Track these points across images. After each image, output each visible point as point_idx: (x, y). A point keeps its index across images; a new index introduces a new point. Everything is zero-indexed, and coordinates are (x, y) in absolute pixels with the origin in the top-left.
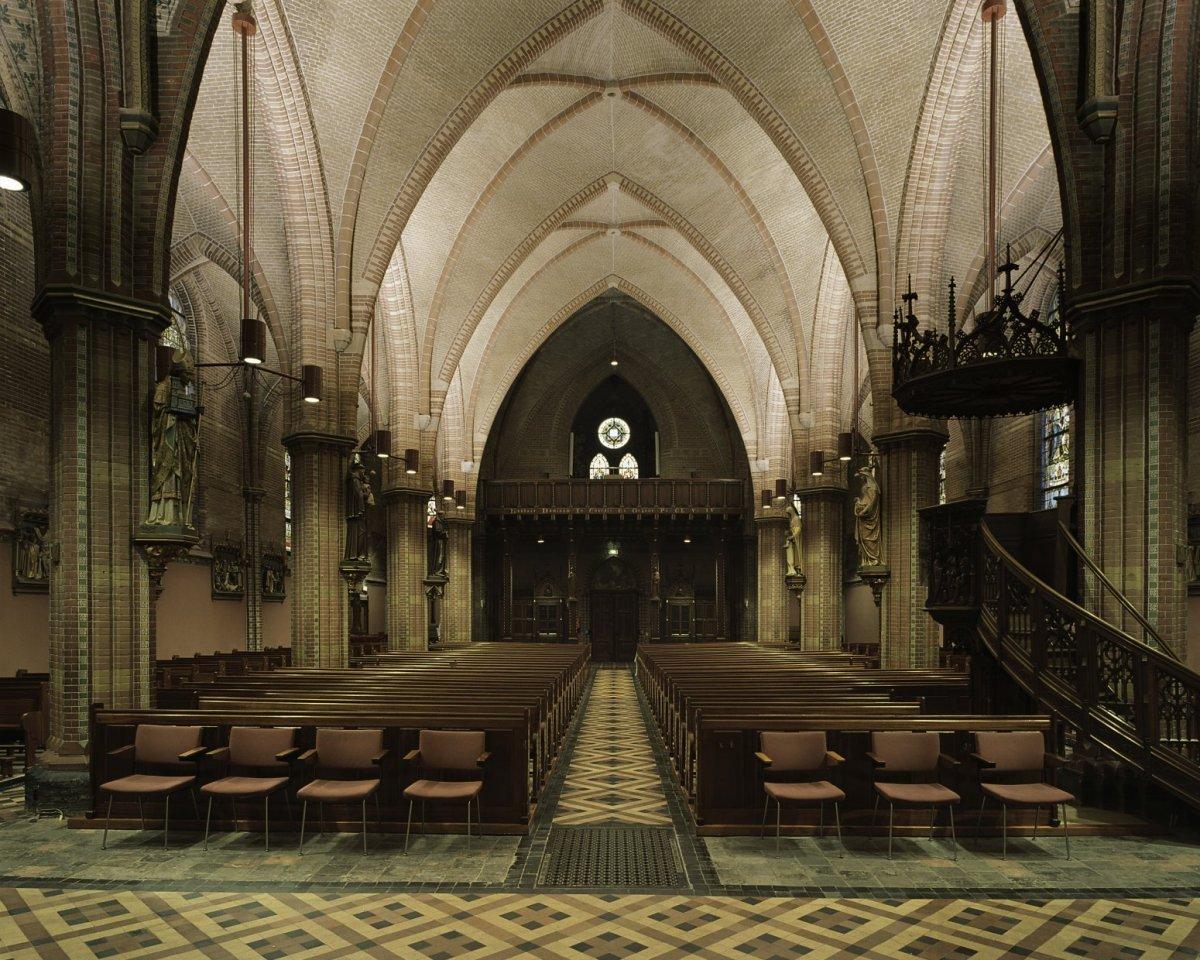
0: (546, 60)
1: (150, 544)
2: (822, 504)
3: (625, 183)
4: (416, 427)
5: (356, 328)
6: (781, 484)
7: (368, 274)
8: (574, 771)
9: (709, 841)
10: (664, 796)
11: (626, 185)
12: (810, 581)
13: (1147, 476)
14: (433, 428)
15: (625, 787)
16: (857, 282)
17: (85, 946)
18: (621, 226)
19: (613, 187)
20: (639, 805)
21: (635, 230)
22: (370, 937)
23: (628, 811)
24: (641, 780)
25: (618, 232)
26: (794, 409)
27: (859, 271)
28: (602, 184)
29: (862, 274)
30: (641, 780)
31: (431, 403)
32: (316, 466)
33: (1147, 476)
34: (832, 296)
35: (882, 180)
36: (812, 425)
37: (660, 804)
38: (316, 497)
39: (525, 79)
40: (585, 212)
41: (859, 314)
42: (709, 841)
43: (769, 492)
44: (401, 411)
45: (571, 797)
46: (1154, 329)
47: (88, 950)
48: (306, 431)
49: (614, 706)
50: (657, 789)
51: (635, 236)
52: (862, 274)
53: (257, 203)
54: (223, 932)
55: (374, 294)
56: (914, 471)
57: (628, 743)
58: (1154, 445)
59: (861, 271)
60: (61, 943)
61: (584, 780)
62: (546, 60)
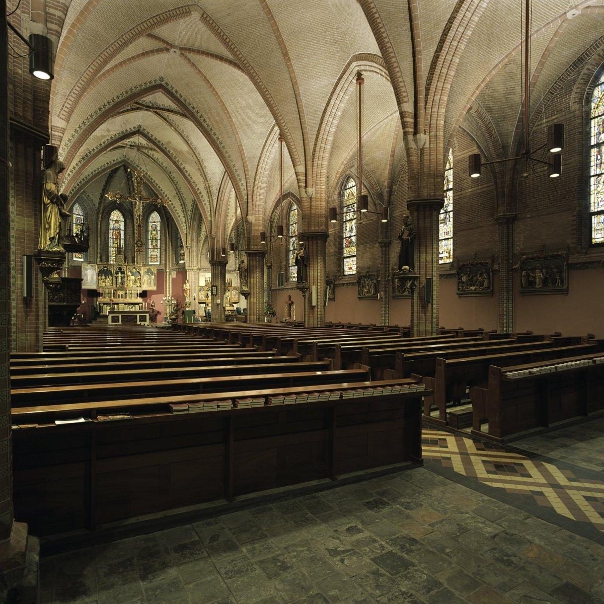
1: (52, 284)
2: (258, 258)
3: (205, 16)
11: (206, 18)
13: (432, 260)
17: (532, 476)
18: (181, 49)
19: (196, 16)
22: (551, 490)
25: (178, 51)
33: (432, 260)
35: (250, 173)
40: (164, 31)
47: (449, 445)
51: (186, 58)
54: (544, 490)
58: (319, 268)
60: (457, 451)
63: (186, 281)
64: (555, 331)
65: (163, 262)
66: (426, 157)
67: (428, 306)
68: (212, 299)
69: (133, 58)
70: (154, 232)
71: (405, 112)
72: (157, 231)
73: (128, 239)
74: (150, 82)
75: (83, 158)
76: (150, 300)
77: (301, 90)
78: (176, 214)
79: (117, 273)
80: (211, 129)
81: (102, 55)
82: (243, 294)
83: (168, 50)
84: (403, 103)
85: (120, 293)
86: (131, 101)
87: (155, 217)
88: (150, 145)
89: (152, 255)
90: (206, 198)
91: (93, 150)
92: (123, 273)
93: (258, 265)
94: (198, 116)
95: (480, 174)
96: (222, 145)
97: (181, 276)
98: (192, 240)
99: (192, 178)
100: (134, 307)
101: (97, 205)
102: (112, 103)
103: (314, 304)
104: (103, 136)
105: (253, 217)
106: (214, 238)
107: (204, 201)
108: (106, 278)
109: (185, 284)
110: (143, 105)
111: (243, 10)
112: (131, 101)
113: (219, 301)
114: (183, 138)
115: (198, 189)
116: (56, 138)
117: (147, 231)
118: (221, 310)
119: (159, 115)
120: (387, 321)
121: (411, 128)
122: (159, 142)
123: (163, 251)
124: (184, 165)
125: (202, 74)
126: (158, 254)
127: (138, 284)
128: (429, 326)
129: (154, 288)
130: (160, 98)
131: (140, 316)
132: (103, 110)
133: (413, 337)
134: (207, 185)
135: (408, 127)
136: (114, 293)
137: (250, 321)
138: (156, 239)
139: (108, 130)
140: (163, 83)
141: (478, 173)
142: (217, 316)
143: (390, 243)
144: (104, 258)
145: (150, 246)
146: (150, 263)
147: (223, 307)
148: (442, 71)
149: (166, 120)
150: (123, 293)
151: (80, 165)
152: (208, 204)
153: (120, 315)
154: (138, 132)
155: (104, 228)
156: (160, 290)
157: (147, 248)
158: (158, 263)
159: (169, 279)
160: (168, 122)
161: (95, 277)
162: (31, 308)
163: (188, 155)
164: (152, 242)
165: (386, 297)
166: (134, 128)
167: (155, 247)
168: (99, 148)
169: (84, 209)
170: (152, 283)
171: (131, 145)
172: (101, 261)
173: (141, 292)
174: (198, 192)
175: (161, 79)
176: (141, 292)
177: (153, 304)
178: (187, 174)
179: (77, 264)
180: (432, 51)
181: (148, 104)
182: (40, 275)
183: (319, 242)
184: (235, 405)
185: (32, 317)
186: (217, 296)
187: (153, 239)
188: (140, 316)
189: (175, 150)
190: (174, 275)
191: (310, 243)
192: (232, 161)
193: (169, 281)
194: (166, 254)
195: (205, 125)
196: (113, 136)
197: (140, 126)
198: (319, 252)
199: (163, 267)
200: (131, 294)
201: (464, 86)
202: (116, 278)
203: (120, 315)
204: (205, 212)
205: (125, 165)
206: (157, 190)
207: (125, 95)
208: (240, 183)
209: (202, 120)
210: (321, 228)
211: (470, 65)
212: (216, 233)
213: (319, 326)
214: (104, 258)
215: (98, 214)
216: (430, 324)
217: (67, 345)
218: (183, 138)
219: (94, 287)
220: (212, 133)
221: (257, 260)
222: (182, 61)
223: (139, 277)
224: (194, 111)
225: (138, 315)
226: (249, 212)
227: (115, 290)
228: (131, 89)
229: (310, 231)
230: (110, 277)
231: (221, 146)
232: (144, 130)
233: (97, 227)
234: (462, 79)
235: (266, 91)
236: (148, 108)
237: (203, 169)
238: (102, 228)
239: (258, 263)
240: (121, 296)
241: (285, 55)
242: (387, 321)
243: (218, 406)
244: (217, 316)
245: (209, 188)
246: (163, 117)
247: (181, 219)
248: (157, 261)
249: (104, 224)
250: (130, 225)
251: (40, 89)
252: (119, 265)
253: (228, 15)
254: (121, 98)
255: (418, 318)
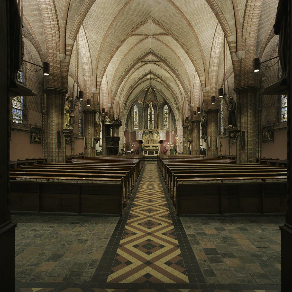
0: (137, 32)
1: (97, 139)
2: (196, 123)
4: (92, 92)
5: (67, 54)
6: (199, 109)
7: (70, 37)
8: (143, 177)
9: (181, 219)
10: (164, 193)
11: (155, 21)
12: (193, 141)
14: (97, 92)
15: (153, 197)
16: (201, 78)
18: (152, 36)
19: (150, 21)
20: (156, 190)
21: (156, 63)
23: (155, 205)
24: (159, 194)
25: (151, 37)
26: (234, 50)
27: (229, 35)
28: (146, 20)
29: (231, 35)
30: (159, 194)
31: (98, 86)
32: (89, 116)
34: (197, 82)
36: (244, 57)
37: (163, 196)
38: (54, 108)
39: (133, 35)
41: (201, 84)
42: (181, 219)
43: (195, 112)
44: (105, 104)
45: (139, 194)
46: (249, 94)
48: (50, 87)
49: (151, 173)
50: (159, 177)
52: (231, 35)
53: (79, 65)
55: (73, 44)
56: (212, 117)
57: (155, 183)
59: (202, 76)
61: (140, 201)
62: (137, 32)
63: (177, 136)
64: (17, 159)
65: (169, 127)
66: (243, 64)
67: (245, 147)
68: (183, 144)
69: (135, 45)
70: (165, 114)
71: (229, 41)
72: (167, 114)
73: (155, 118)
74: (146, 52)
75: (129, 88)
76: (164, 144)
77: (200, 39)
78: (171, 104)
79: (150, 133)
80: (173, 66)
81: (114, 50)
82: (189, 141)
83: (147, 38)
84: (228, 37)
85: (151, 142)
86: (142, 60)
87: (166, 107)
88: (155, 77)
89: (165, 124)
90: (180, 97)
91: (133, 84)
92: (152, 133)
93: (196, 127)
94: (167, 61)
95: (260, 70)
96: (178, 72)
97: (175, 133)
98: (179, 116)
99: (173, 89)
100: (156, 148)
101: (143, 105)
102: (131, 65)
103: (209, 146)
104: (136, 78)
105: (194, 104)
106: (184, 115)
107: (179, 98)
108: (145, 136)
109: (176, 137)
110: (148, 62)
111: (169, 11)
112: (142, 60)
113: (186, 145)
114: (167, 71)
115: (176, 93)
116: (236, 61)
117: (163, 114)
118: (187, 149)
119: (155, 64)
120: (260, 155)
121: (234, 49)
122: (159, 75)
123: (169, 122)
124: (170, 83)
125: (164, 43)
126: (167, 124)
127: (158, 138)
128: (246, 158)
129: (165, 139)
130: (150, 57)
131: (144, 152)
132: (128, 68)
133: (237, 163)
134: (180, 91)
135: (232, 49)
136: (149, 142)
137: (193, 154)
138: (166, 117)
139: (138, 75)
140: (152, 51)
141: (258, 69)
142: (185, 152)
143: (261, 110)
144: (146, 127)
145: (164, 121)
146: (164, 128)
147: (188, 148)
148: (250, 13)
149: (159, 65)
150: (152, 141)
151: (128, 91)
152: (181, 99)
153: (147, 151)
154: (150, 73)
155: (145, 114)
156: (168, 139)
157: (163, 122)
158: (167, 128)
159: (171, 135)
160: (160, 66)
161: (141, 135)
162: (61, 149)
163: (171, 79)
164: (165, 119)
165: (259, 141)
166: (148, 71)
167: (166, 121)
168: (135, 82)
169: (138, 107)
170: (164, 137)
171: (150, 79)
172: (145, 128)
173: (159, 141)
174: (176, 95)
175: (150, 49)
176: (159, 141)
177: (165, 146)
178: (171, 87)
179: (135, 130)
180: (244, 3)
181: (150, 61)
182: (64, 137)
183: (212, 114)
184: (48, 181)
185: (61, 152)
186: (185, 142)
187: (165, 117)
188: (144, 152)
189: (165, 77)
190: (173, 133)
191: (208, 115)
192: (183, 79)
193: (171, 136)
194: (170, 123)
195: (170, 65)
196: (140, 77)
197: (151, 70)
198: (212, 119)
199: (169, 130)
200: (155, 142)
201: (269, 15)
202: (150, 135)
203: (147, 151)
204: (179, 104)
205: (151, 87)
206: (164, 96)
207: (136, 60)
208: (187, 89)
209: (168, 63)
210: (213, 107)
211: (271, 2)
212: (185, 113)
213: (212, 157)
214: (146, 127)
215: (143, 109)
216: (246, 157)
217: (73, 161)
218: (167, 71)
219: (141, 139)
220: (173, 68)
221: (196, 125)
222: (154, 40)
223: (159, 135)
224: (165, 60)
225: (155, 151)
226: (191, 102)
227: (149, 141)
228: (139, 57)
229: (208, 109)
230: (147, 135)
231: (177, 73)
232: (152, 71)
233: (143, 114)
234: (267, 12)
235: (183, 45)
236: (150, 62)
237: (177, 84)
238: (145, 114)
239: (196, 126)
240: (151, 143)
241: (190, 24)
242: (260, 155)
243: (30, 180)
244: (185, 152)
245: (181, 92)
246: (157, 64)
247: (174, 108)
248: (167, 127)
249: (146, 113)
250: (156, 112)
251: (64, 75)
252: (150, 130)
253: (163, 16)
254: (135, 62)
255: (239, 153)
